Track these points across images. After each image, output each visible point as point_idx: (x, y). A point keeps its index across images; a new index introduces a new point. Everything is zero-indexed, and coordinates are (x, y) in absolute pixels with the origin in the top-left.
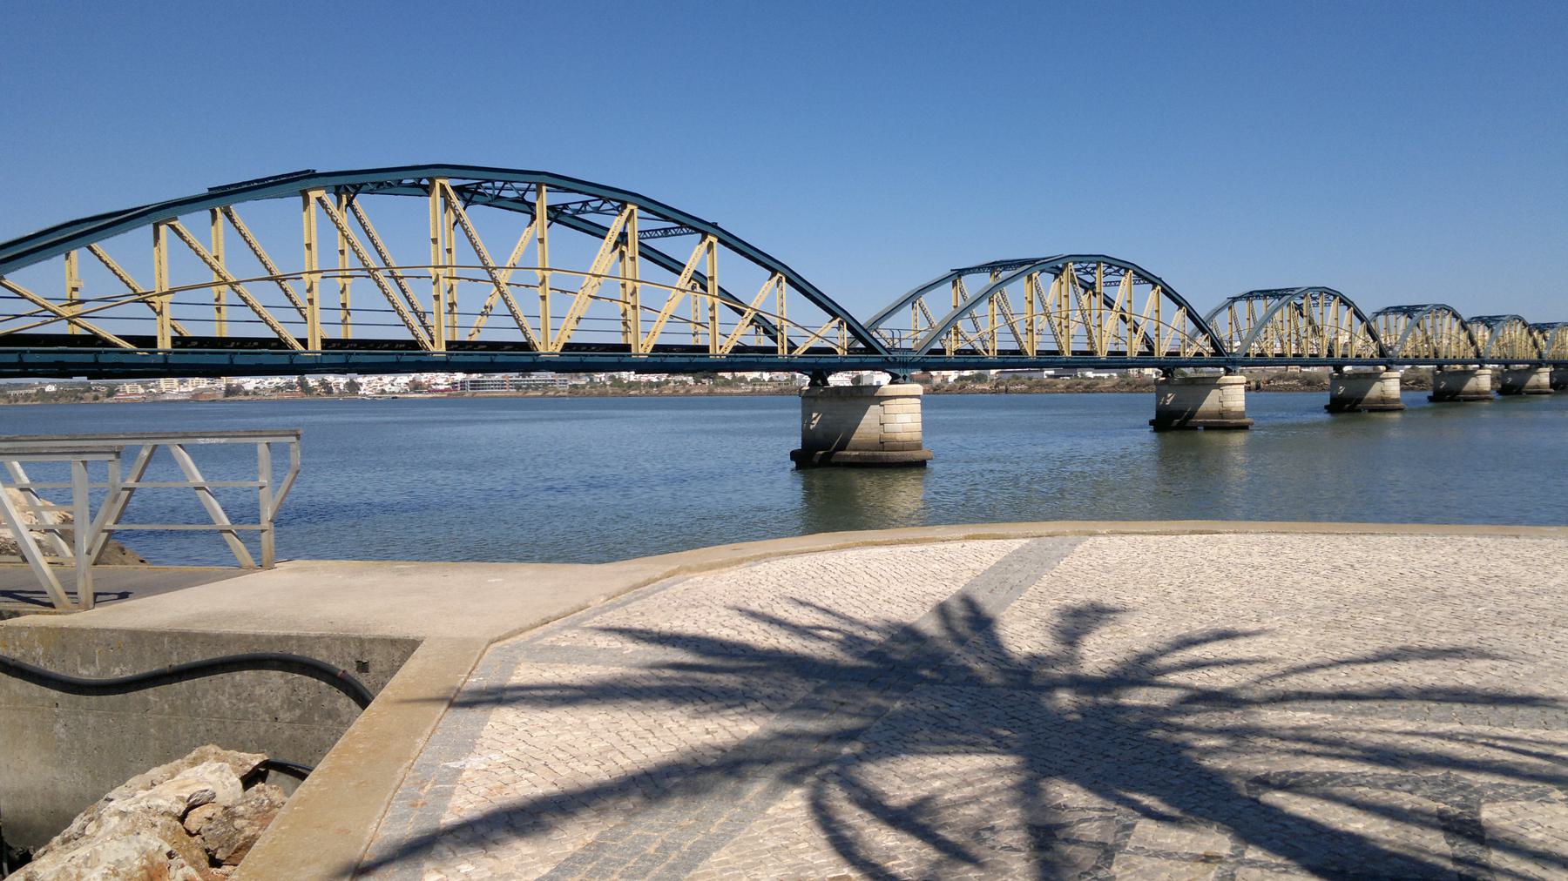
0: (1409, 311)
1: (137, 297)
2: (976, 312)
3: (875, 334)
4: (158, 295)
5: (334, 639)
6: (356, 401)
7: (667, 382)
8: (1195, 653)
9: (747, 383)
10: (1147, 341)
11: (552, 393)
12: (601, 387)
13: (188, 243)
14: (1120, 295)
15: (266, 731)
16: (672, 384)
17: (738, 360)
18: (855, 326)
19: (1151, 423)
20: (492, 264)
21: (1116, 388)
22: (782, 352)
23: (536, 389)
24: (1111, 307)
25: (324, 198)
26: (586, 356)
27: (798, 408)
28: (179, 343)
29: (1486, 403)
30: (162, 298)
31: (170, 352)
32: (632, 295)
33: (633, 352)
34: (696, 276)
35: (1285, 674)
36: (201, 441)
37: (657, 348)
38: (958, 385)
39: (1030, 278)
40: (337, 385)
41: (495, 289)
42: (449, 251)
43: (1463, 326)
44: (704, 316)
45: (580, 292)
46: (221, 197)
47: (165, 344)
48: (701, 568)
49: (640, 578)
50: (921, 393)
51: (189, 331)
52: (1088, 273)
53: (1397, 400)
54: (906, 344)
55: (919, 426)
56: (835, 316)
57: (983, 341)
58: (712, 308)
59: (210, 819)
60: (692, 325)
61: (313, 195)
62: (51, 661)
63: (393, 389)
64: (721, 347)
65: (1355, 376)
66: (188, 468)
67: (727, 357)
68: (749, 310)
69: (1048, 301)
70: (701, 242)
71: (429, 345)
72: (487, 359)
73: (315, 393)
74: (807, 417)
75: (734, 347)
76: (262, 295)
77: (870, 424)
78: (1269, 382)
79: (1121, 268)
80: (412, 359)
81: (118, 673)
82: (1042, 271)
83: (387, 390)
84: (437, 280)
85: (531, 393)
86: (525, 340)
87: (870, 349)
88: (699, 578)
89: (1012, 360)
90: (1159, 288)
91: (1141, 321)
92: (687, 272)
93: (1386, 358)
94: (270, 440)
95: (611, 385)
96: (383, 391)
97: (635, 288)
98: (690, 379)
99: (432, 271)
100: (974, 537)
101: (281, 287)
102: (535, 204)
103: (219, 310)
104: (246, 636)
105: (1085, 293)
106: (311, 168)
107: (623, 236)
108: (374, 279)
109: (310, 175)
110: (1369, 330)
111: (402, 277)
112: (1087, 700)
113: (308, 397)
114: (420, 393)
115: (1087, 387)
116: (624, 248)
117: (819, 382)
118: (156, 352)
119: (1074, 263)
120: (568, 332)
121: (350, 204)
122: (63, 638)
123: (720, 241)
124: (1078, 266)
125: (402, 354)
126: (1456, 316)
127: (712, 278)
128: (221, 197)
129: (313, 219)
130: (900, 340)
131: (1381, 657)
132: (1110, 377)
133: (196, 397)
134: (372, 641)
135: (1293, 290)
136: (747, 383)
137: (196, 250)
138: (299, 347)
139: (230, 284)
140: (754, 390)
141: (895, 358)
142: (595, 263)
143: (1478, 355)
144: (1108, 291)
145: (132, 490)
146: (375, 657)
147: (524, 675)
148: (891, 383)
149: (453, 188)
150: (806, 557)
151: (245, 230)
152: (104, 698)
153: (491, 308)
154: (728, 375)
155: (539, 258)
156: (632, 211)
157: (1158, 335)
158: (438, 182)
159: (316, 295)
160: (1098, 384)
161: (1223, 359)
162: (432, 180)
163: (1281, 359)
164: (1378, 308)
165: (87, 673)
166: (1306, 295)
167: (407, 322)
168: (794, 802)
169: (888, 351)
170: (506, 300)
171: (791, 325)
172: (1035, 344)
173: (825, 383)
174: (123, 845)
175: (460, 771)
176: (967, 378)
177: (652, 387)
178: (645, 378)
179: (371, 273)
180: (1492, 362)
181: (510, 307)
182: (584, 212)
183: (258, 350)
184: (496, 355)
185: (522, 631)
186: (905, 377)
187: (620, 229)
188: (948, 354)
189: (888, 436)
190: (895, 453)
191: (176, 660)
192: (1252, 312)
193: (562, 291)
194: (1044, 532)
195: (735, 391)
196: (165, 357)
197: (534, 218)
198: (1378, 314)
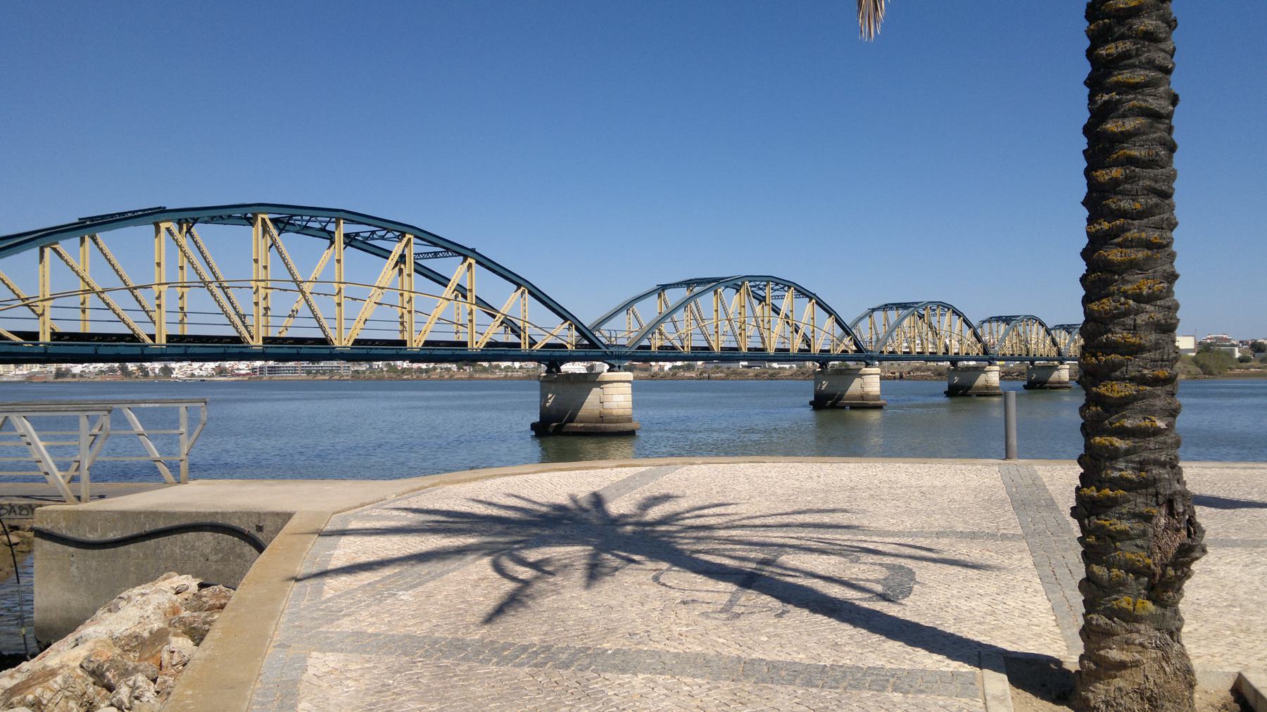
0: (1007, 320)
1: (27, 302)
2: (675, 316)
3: (597, 334)
4: (42, 301)
5: (243, 513)
6: (169, 383)
7: (434, 369)
8: (706, 512)
9: (501, 369)
10: (806, 340)
11: (337, 377)
12: (379, 372)
13: (66, 261)
14: (784, 305)
15: (201, 567)
16: (439, 370)
17: (490, 353)
18: (581, 327)
19: (811, 403)
20: (300, 279)
21: (793, 376)
22: (525, 347)
23: (324, 374)
24: (779, 314)
25: (171, 228)
26: (371, 349)
27: (1052, 454)
28: (55, 337)
29: (1067, 391)
30: (45, 303)
31: (49, 344)
32: (408, 302)
33: (408, 346)
34: (459, 288)
35: (744, 519)
36: (143, 405)
37: (427, 343)
38: (671, 373)
39: (716, 292)
40: (153, 369)
41: (301, 296)
42: (265, 267)
43: (1048, 332)
44: (464, 319)
45: (368, 300)
46: (88, 226)
47: (45, 338)
48: (453, 482)
49: (416, 486)
50: (632, 379)
51: (61, 328)
52: (761, 289)
53: (997, 388)
54: (620, 342)
55: (630, 404)
56: (566, 320)
57: (681, 340)
58: (471, 313)
59: (186, 599)
60: (455, 326)
61: (163, 226)
62: (70, 530)
63: (201, 373)
64: (477, 343)
65: (1043, 367)
66: (134, 422)
67: (482, 350)
68: (499, 315)
69: (730, 312)
70: (462, 263)
71: (250, 340)
72: (294, 351)
73: (133, 376)
74: (544, 397)
75: (487, 343)
76: (120, 300)
77: (592, 403)
78: (909, 373)
79: (785, 286)
80: (237, 350)
81: (111, 536)
82: (726, 287)
83: (196, 374)
84: (257, 290)
85: (320, 377)
86: (324, 337)
87: (593, 345)
88: (451, 487)
89: (703, 353)
90: (814, 301)
91: (801, 326)
92: (452, 285)
93: (988, 357)
94: (188, 405)
95: (387, 371)
96: (193, 375)
97: (411, 298)
98: (454, 367)
99: (253, 284)
100: (621, 466)
101: (133, 294)
102: (334, 233)
103: (84, 311)
104: (191, 513)
105: (760, 304)
106: (163, 205)
107: (402, 257)
108: (208, 289)
109: (162, 210)
110: (975, 334)
111: (228, 288)
112: (639, 529)
113: (127, 380)
114: (225, 376)
115: (772, 375)
116: (403, 266)
117: (554, 370)
118: (38, 344)
119: (750, 282)
120: (358, 331)
121: (189, 231)
122: (79, 517)
123: (478, 262)
124: (753, 284)
125: (229, 347)
126: (1042, 324)
127: (471, 290)
128: (88, 226)
129: (163, 244)
130: (616, 338)
131: (794, 513)
132: (791, 367)
133: (30, 378)
134: (265, 514)
135: (917, 303)
136: (501, 370)
137: (71, 267)
138: (149, 341)
139: (97, 293)
140: (506, 376)
141: (612, 352)
142: (380, 278)
143: (1059, 353)
144: (776, 302)
145: (96, 436)
146: (267, 523)
147: (354, 525)
148: (609, 371)
149: (271, 220)
150: (517, 476)
151: (107, 250)
152: (103, 551)
153: (297, 311)
154: (486, 364)
155: (336, 274)
156: (409, 239)
157: (813, 337)
158: (260, 217)
159: (163, 301)
160: (779, 373)
161: (864, 356)
162: (255, 215)
163: (908, 356)
164: (984, 318)
165: (92, 537)
166: (926, 307)
167: (233, 323)
168: (486, 561)
169: (607, 346)
170: (310, 306)
171: (531, 326)
172: (718, 343)
173: (559, 370)
174: (161, 596)
175: (332, 555)
176: (679, 368)
177: (422, 373)
178: (415, 365)
179: (205, 284)
180: (1004, 358)
181: (313, 311)
182: (373, 239)
183: (118, 343)
184: (301, 348)
185: (350, 509)
186: (619, 367)
187: (400, 252)
188: (653, 349)
189: (605, 411)
190: (612, 425)
191: (148, 528)
192: (887, 319)
193: (352, 299)
194: (664, 463)
195: (490, 376)
196: (45, 348)
197: (332, 242)
198: (984, 322)
